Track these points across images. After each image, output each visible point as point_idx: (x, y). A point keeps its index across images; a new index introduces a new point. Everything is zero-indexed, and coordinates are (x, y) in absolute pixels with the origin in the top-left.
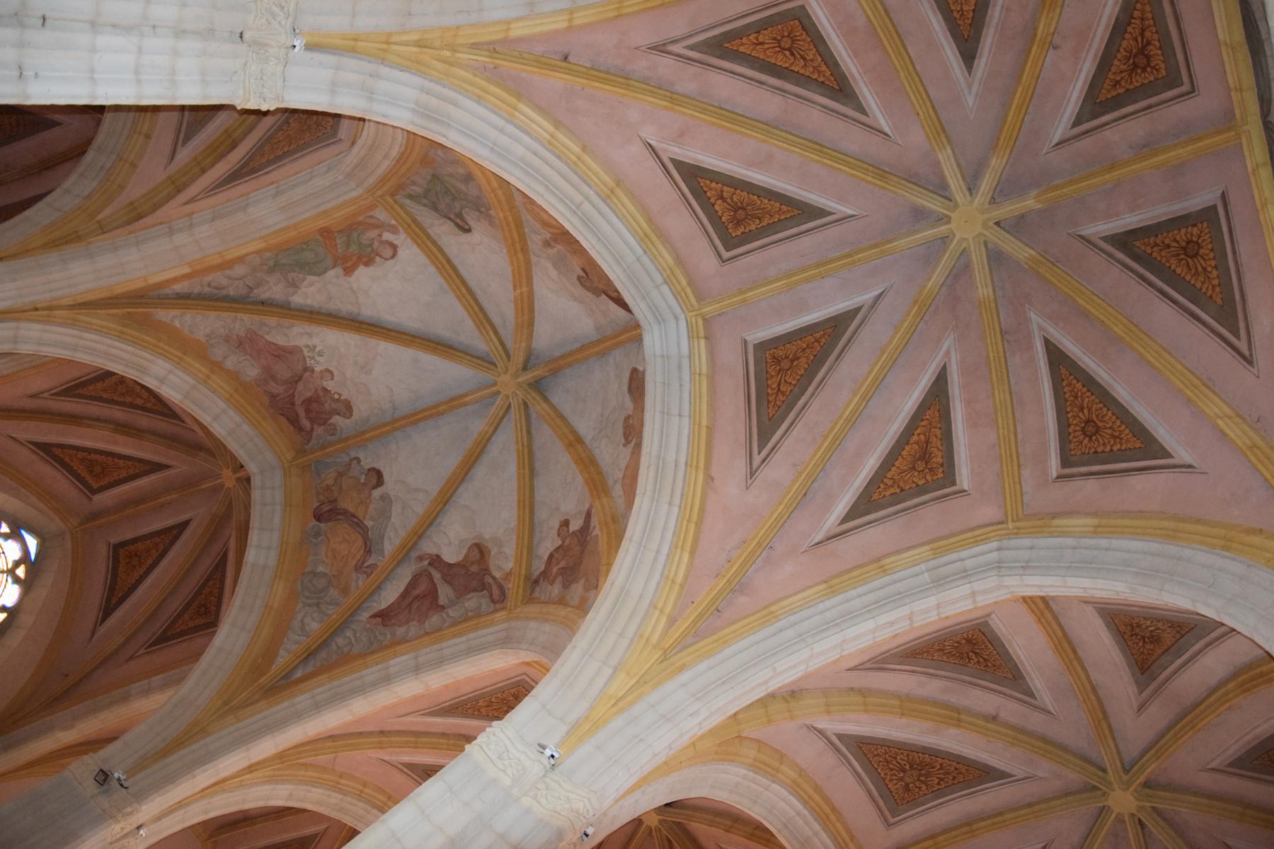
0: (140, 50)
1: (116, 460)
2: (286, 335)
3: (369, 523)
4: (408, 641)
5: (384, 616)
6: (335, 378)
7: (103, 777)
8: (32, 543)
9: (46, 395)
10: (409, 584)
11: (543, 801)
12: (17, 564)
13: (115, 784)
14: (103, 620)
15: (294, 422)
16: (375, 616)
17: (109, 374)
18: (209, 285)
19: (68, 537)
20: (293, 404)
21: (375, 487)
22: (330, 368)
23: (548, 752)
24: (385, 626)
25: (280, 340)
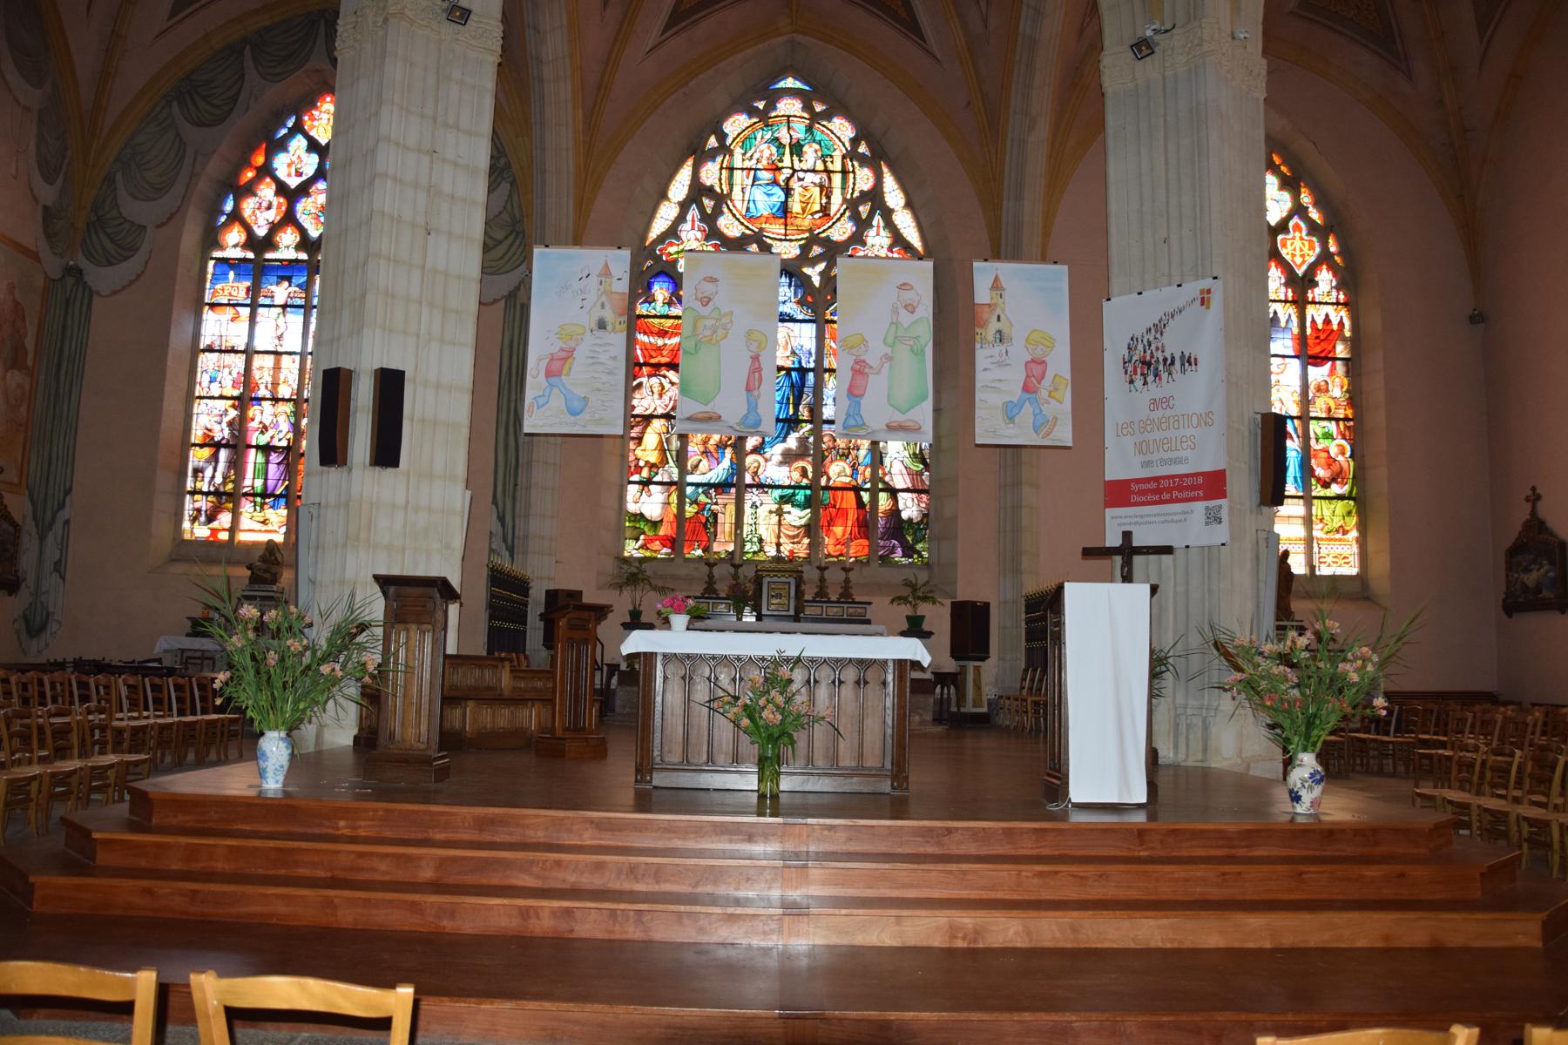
8: (790, 83)
12: (807, 107)
14: (922, 37)
19: (799, 38)
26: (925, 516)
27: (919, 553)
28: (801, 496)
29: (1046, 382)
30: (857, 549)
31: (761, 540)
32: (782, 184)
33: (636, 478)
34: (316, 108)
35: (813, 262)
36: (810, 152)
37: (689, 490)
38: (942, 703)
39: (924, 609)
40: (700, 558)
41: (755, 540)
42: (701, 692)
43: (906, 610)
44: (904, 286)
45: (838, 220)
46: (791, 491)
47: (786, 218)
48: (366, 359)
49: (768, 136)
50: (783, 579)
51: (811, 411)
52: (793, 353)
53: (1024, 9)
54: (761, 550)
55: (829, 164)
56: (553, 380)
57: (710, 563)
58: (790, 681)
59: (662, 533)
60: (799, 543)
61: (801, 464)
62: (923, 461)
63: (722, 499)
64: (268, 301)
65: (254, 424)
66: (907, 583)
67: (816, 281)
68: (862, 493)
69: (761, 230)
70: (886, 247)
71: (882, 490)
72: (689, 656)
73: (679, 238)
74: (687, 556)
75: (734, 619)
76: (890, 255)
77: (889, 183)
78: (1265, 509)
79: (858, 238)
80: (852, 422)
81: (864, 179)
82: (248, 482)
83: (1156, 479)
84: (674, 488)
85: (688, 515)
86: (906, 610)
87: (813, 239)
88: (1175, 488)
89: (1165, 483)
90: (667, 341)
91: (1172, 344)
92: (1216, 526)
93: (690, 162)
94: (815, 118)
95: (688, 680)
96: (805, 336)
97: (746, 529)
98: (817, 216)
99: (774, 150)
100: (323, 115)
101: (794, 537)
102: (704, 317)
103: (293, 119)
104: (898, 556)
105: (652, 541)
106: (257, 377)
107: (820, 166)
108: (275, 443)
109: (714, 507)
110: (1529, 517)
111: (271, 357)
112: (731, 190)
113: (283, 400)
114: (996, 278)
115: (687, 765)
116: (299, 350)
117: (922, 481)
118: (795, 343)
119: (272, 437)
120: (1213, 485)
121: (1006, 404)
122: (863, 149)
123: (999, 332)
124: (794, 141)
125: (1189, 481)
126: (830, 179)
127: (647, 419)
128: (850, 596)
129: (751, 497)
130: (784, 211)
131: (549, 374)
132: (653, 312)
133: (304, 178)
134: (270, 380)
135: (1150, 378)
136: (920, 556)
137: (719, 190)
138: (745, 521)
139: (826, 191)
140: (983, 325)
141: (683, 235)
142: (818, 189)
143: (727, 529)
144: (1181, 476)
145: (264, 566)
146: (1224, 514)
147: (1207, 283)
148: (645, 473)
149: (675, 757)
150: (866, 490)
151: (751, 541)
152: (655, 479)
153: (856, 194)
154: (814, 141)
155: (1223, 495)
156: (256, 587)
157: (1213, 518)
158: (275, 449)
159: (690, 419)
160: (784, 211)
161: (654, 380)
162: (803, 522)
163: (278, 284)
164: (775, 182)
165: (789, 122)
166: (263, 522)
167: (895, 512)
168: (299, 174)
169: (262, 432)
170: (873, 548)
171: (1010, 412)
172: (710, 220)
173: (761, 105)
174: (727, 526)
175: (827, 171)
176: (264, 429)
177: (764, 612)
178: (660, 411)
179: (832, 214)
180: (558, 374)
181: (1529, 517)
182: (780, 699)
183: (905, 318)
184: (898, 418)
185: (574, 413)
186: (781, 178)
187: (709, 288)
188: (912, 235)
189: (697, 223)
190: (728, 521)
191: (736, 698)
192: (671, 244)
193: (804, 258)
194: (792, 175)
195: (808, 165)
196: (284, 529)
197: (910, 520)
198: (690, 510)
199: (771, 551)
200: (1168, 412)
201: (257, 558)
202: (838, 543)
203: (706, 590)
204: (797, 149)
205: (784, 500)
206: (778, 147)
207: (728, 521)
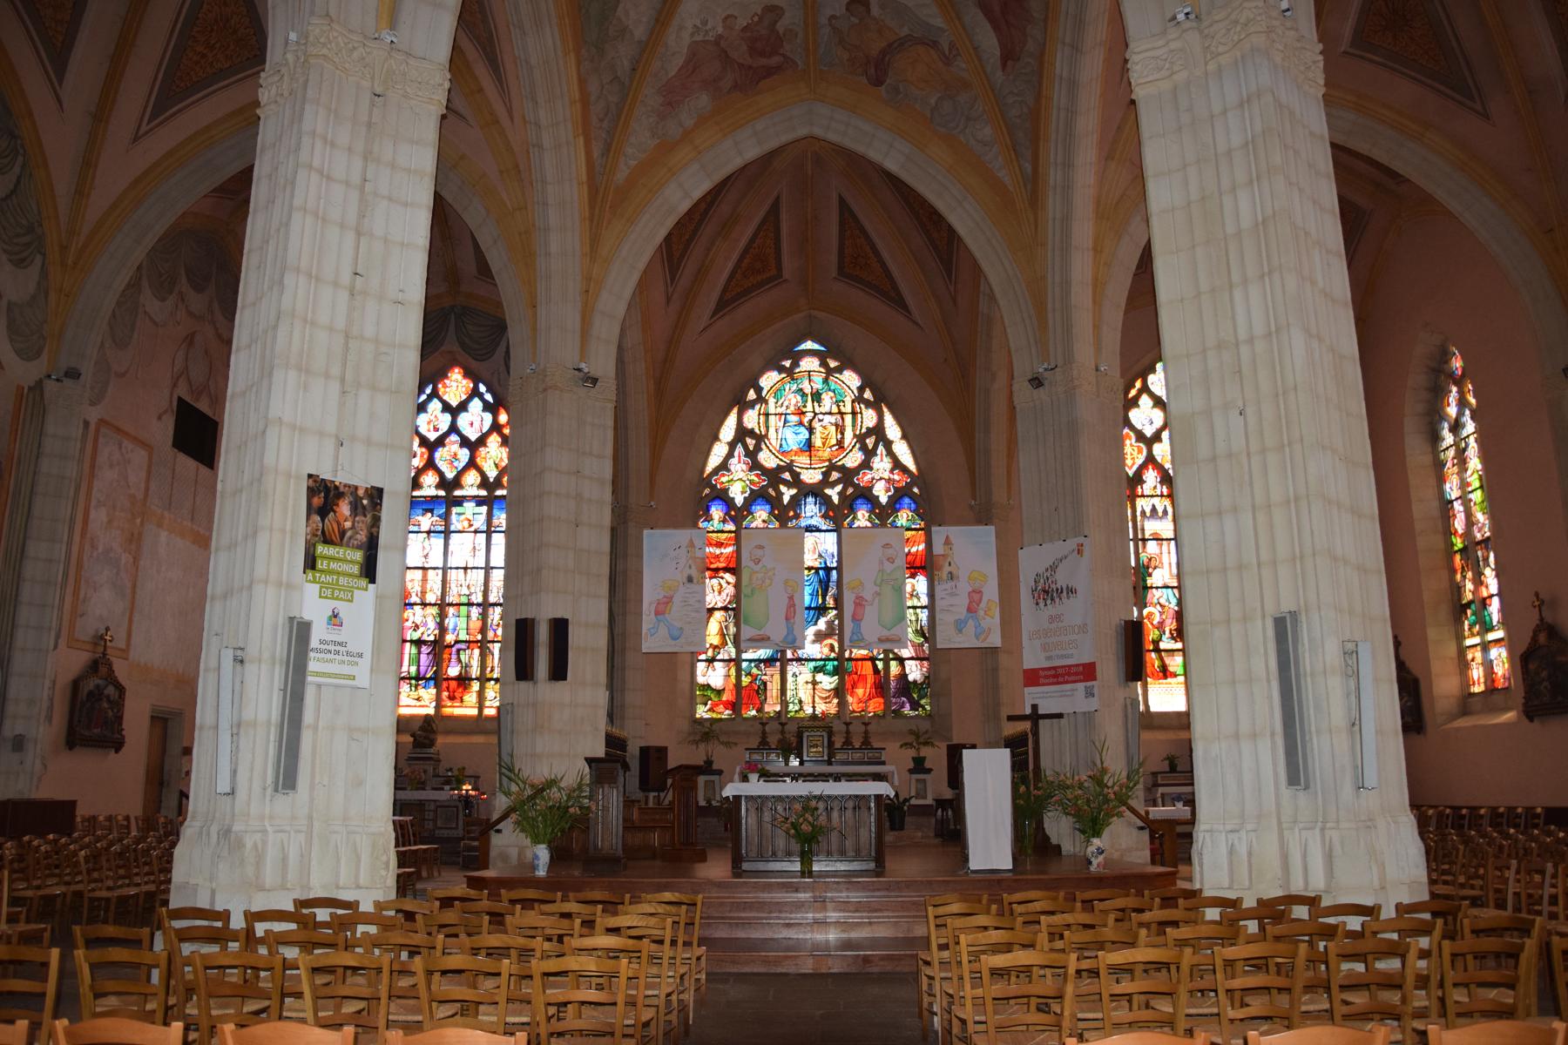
0: (266, 582)
1: (755, 245)
2: (673, 54)
3: (905, 31)
4: (1044, 44)
5: (1009, 56)
6: (736, 14)
7: (1037, 382)
8: (809, 345)
9: (671, 290)
10: (985, 15)
11: (1221, 49)
12: (824, 364)
13: (1047, 374)
15: (769, 72)
16: (1004, 66)
17: (668, 238)
18: (601, 120)
20: (750, 67)
21: (869, 11)
22: (723, 17)
23: (1181, 17)
24: (1019, 59)
25: (679, 61)
26: (926, 678)
27: (923, 707)
28: (830, 666)
29: (983, 605)
30: (876, 706)
31: (800, 702)
32: (806, 424)
33: (703, 657)
34: (447, 377)
35: (833, 485)
36: (827, 399)
37: (744, 665)
38: (942, 823)
39: (926, 752)
40: (755, 717)
41: (796, 701)
42: (767, 817)
43: (912, 753)
44: (887, 546)
45: (851, 450)
46: (822, 663)
47: (810, 451)
48: (545, 611)
49: (794, 387)
50: (819, 733)
51: (836, 600)
52: (820, 556)
53: (981, 296)
54: (801, 709)
55: (842, 408)
56: (659, 617)
57: (762, 721)
58: (817, 809)
59: (724, 699)
60: (830, 702)
61: (829, 641)
62: (923, 635)
63: (769, 671)
64: (416, 529)
65: (408, 624)
66: (911, 732)
67: (836, 499)
68: (877, 662)
69: (792, 461)
70: (888, 470)
71: (892, 659)
72: (759, 797)
73: (729, 470)
74: (745, 716)
75: (783, 764)
76: (891, 476)
77: (889, 420)
78: (1130, 684)
79: (866, 465)
80: (855, 638)
81: (869, 418)
82: (405, 668)
83: (1054, 668)
84: (732, 663)
85: (744, 684)
86: (912, 753)
87: (832, 467)
88: (1066, 674)
89: (1060, 671)
90: (723, 550)
91: (1061, 579)
92: (1091, 699)
93: (735, 410)
94: (830, 372)
95: (759, 810)
96: (828, 542)
97: (789, 693)
98: (834, 448)
99: (799, 398)
100: (453, 383)
101: (826, 698)
102: (757, 572)
103: (431, 387)
104: (907, 710)
105: (717, 705)
106: (409, 588)
107: (835, 410)
108: (425, 638)
109: (763, 677)
110: (1538, 622)
111: (420, 571)
112: (768, 430)
113: (430, 604)
114: (947, 537)
115: (761, 857)
116: (441, 566)
117: (923, 651)
118: (821, 548)
119: (422, 634)
120: (1087, 672)
121: (956, 621)
122: (868, 395)
123: (951, 573)
124: (814, 391)
125: (1074, 670)
126: (843, 419)
127: (711, 611)
128: (869, 743)
129: (792, 668)
130: (809, 446)
131: (657, 613)
132: (712, 529)
133: (440, 433)
134: (419, 589)
135: (1049, 602)
136: (924, 709)
137: (758, 432)
138: (788, 687)
139: (840, 428)
140: (940, 569)
141: (732, 468)
142: (834, 428)
143: (774, 694)
144: (1069, 666)
145: (424, 734)
146: (1096, 691)
147: (1081, 540)
148: (710, 653)
149: (753, 854)
150: (880, 660)
151: (793, 703)
152: (718, 658)
153: (864, 430)
154: (830, 390)
155: (1094, 679)
156: (419, 750)
157: (1090, 693)
158: (425, 642)
159: (749, 640)
160: (809, 446)
161: (715, 581)
162: (833, 686)
163: (423, 515)
164: (801, 424)
165: (809, 376)
166: (418, 699)
167: (903, 676)
168: (436, 429)
169: (415, 630)
170: (887, 704)
171: (959, 626)
172: (752, 455)
173: (787, 364)
174: (774, 691)
175: (841, 413)
176: (416, 627)
177: (805, 758)
178: (720, 605)
179: (846, 446)
180: (663, 613)
181: (1538, 622)
182: (810, 819)
183: (888, 567)
184: (885, 633)
185: (675, 639)
186: (806, 420)
187: (759, 552)
188: (908, 460)
189: (742, 458)
190: (775, 687)
191: (787, 819)
192: (723, 475)
193: (826, 482)
194: (814, 418)
195: (826, 409)
196: (434, 704)
197: (915, 681)
198: (745, 680)
199: (809, 710)
200: (1060, 624)
201: (417, 728)
202: (860, 701)
203: (760, 743)
204: (817, 396)
205: (817, 670)
206: (802, 396)
207: (775, 687)
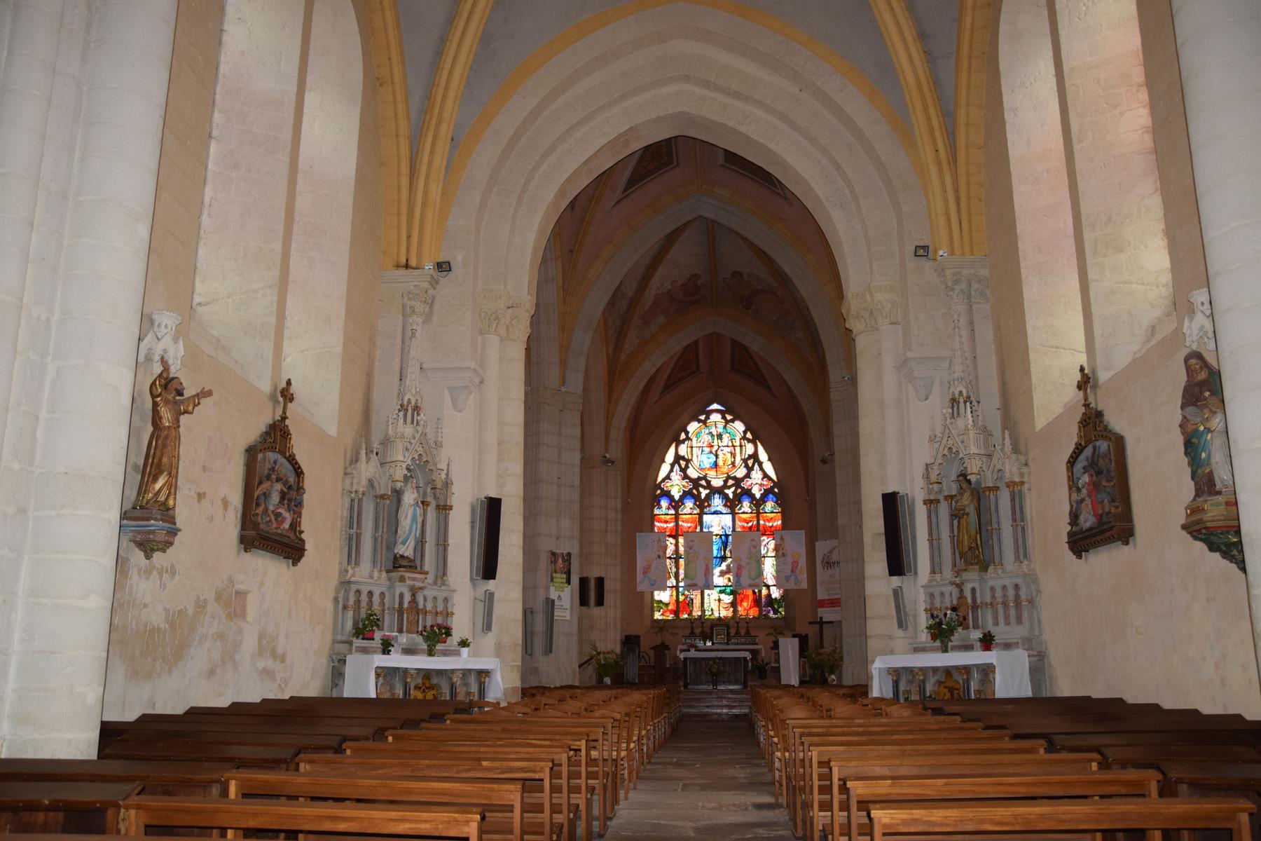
8: (715, 406)
